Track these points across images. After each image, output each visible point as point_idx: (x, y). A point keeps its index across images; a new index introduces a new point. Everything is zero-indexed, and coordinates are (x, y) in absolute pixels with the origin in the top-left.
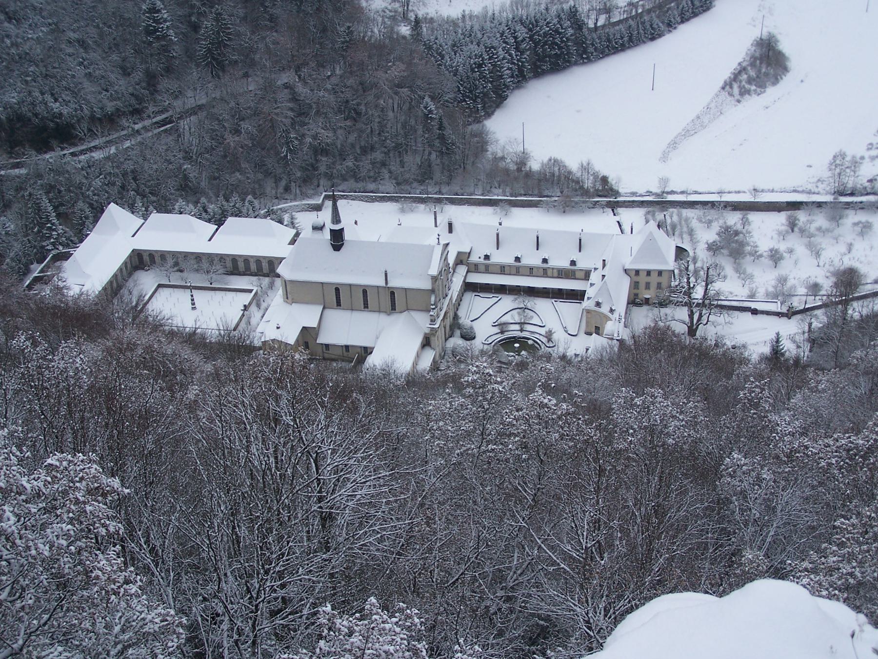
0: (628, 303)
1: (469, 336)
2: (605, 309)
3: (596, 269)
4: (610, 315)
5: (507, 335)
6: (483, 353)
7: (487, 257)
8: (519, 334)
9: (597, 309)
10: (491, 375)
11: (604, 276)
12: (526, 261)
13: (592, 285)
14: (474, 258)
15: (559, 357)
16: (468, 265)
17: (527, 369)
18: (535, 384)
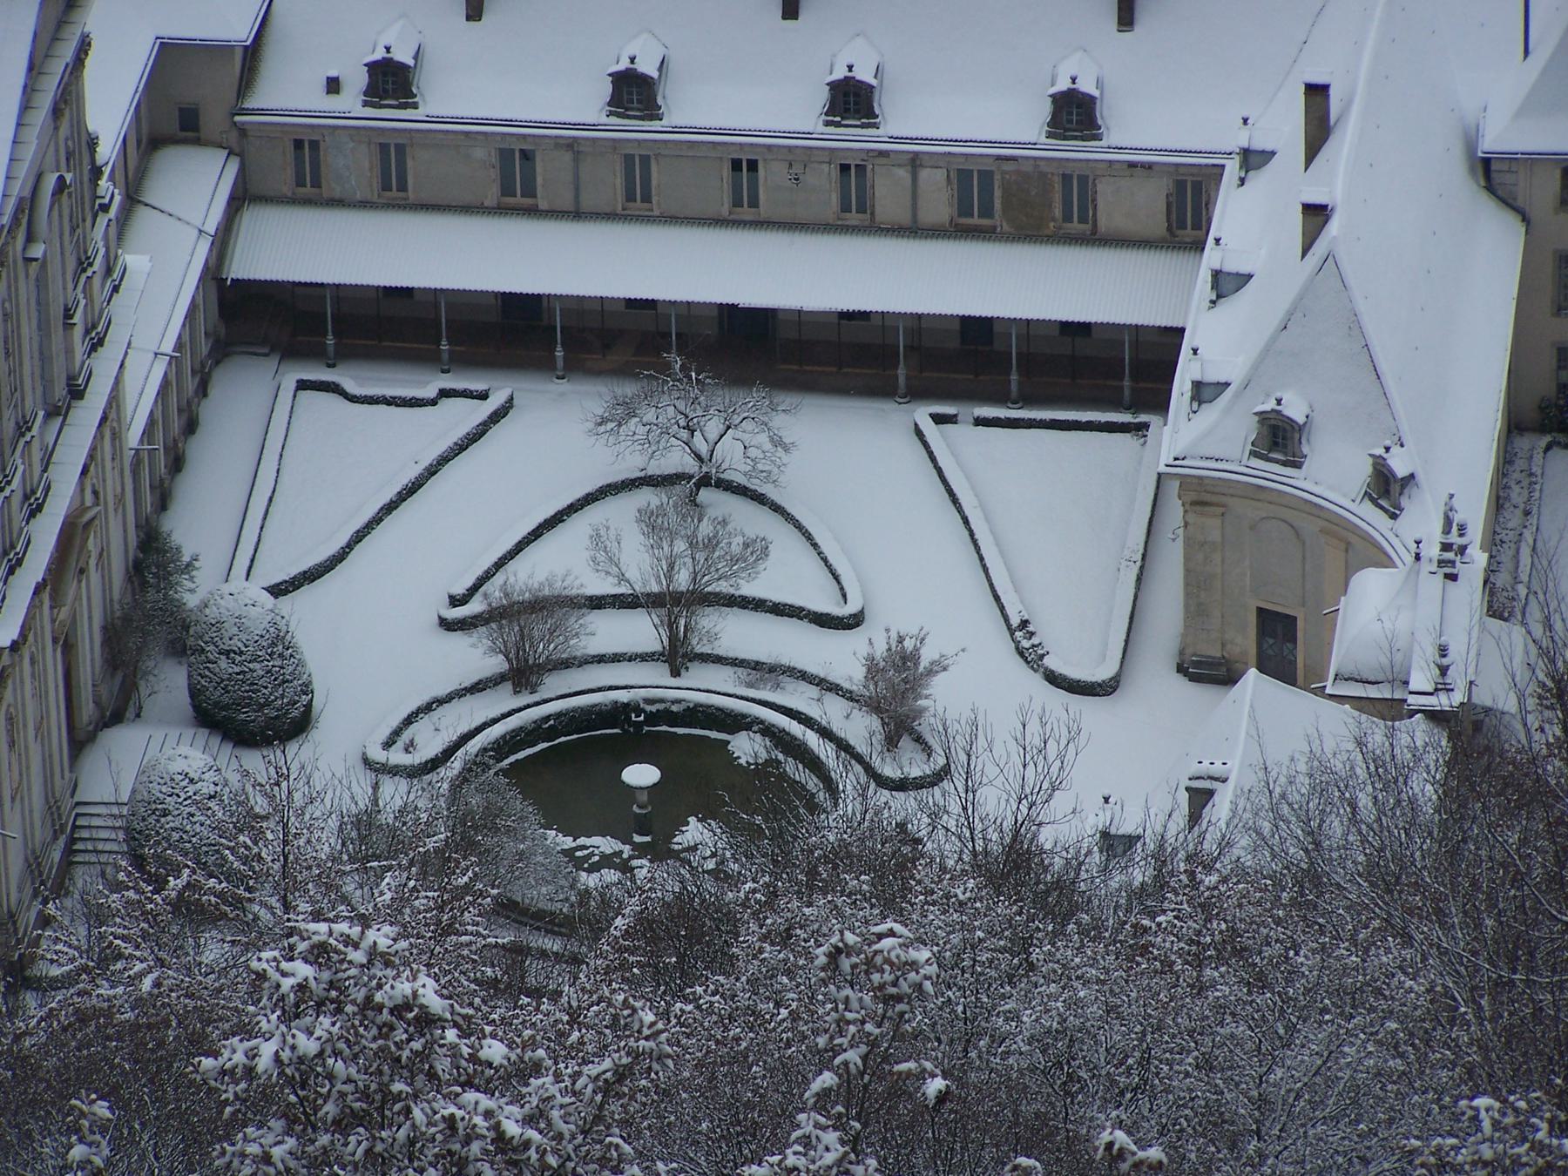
0: (1515, 425)
1: (257, 709)
2: (1332, 475)
3: (1253, 159)
4: (1371, 517)
5: (563, 693)
6: (370, 840)
7: (391, 80)
8: (648, 683)
9: (1270, 472)
10: (427, 1021)
11: (1316, 214)
12: (700, 106)
13: (1225, 284)
14: (290, 90)
15: (980, 864)
16: (240, 143)
17: (727, 964)
18: (791, 1076)
